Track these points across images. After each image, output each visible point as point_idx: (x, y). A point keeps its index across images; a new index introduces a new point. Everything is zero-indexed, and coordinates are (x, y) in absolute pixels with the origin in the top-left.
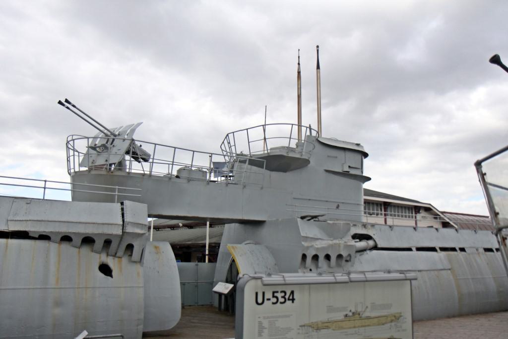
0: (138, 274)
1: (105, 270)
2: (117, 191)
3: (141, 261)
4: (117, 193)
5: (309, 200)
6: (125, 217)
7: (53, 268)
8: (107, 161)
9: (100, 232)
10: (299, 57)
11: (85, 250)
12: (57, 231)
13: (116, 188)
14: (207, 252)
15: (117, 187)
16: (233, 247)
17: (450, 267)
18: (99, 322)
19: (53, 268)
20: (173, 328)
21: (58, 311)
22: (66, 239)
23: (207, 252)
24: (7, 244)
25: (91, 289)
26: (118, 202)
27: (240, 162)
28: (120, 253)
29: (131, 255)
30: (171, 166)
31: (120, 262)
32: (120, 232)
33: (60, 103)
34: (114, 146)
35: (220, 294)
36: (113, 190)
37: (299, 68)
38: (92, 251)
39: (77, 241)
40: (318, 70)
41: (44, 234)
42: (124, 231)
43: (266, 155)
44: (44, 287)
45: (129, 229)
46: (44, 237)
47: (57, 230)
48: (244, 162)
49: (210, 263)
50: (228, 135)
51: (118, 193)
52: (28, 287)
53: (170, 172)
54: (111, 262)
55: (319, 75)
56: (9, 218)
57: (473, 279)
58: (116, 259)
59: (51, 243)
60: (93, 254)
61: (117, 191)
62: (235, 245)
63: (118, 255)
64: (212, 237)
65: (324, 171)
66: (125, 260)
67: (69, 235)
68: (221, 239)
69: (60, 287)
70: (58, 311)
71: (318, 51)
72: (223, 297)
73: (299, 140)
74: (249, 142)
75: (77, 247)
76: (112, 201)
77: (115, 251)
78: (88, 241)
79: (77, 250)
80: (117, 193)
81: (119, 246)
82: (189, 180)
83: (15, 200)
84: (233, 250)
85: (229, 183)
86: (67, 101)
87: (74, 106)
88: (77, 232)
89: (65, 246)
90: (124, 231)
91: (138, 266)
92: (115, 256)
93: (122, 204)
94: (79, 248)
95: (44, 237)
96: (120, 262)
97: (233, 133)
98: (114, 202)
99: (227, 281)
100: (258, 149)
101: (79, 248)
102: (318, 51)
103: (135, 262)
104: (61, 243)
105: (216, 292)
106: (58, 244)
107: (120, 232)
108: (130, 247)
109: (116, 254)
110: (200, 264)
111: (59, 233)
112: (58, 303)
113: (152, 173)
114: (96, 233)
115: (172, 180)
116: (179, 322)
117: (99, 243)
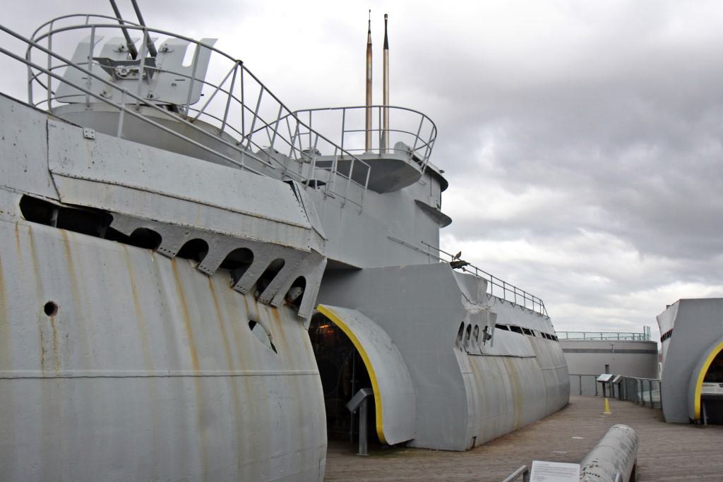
5: (402, 243)
10: (369, 21)
12: (185, 224)
17: (534, 355)
19: (179, 325)
30: (382, 109)
31: (277, 316)
35: (604, 383)
37: (369, 39)
38: (232, 287)
40: (386, 50)
41: (151, 227)
43: (376, 158)
44: (173, 372)
46: (146, 239)
47: (183, 221)
53: (313, 145)
55: (370, 66)
57: (556, 369)
59: (155, 254)
65: (414, 202)
66: (284, 312)
71: (386, 21)
73: (366, 150)
74: (343, 131)
88: (228, 233)
89: (187, 266)
92: (269, 304)
95: (146, 239)
97: (344, 108)
100: (355, 146)
102: (386, 21)
105: (600, 381)
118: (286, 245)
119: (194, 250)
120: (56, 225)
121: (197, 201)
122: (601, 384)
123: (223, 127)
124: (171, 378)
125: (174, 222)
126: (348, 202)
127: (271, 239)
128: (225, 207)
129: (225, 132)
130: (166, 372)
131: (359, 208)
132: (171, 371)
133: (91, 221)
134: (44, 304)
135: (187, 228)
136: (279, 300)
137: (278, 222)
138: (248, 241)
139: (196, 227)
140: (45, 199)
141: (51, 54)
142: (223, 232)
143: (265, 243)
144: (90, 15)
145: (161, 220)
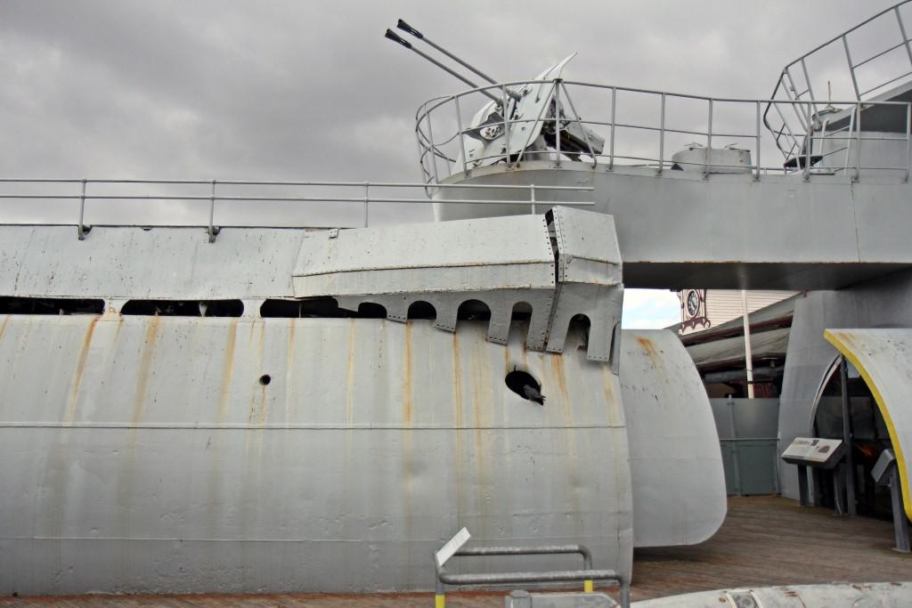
0: (608, 393)
1: (521, 382)
2: (533, 195)
3: (611, 361)
4: (533, 201)
6: (559, 245)
7: (395, 384)
8: (504, 150)
9: (500, 287)
11: (470, 338)
12: (398, 291)
13: (530, 189)
14: (750, 378)
15: (532, 186)
16: (843, 336)
18: (516, 515)
20: (701, 544)
21: (414, 485)
22: (421, 311)
23: (750, 378)
24: (293, 327)
25: (489, 432)
26: (537, 212)
27: (830, 128)
28: (557, 342)
29: (584, 348)
31: (558, 366)
32: (550, 283)
33: (390, 35)
34: (517, 117)
35: (802, 464)
36: (525, 194)
39: (448, 313)
42: (560, 280)
45: (572, 274)
46: (371, 310)
48: (843, 124)
49: (758, 400)
50: (787, 68)
51: (536, 199)
52: (341, 425)
54: (535, 365)
56: (295, 273)
58: (549, 357)
59: (387, 322)
60: (490, 347)
61: (533, 195)
62: (846, 331)
63: (550, 347)
64: (757, 347)
66: (570, 360)
67: (423, 299)
68: (786, 344)
69: (415, 426)
70: (414, 485)
72: (809, 470)
75: (449, 332)
76: (525, 210)
77: (543, 337)
78: (473, 313)
79: (451, 337)
80: (533, 201)
81: (552, 316)
82: (708, 174)
83: (307, 234)
84: (845, 343)
85: (811, 174)
86: (402, 25)
87: (419, 35)
89: (420, 329)
90: (560, 280)
91: (606, 373)
92: (543, 349)
93: (550, 217)
94: (455, 333)
95: (371, 310)
96: (558, 366)
98: (531, 213)
99: (817, 433)
101: (455, 333)
103: (596, 364)
104: (411, 323)
105: (789, 460)
106: (402, 326)
107: (550, 283)
108: (580, 325)
109: (546, 344)
110: (738, 401)
111: (402, 296)
112: (413, 467)
113: (615, 159)
114: (490, 288)
115: (665, 175)
116: (725, 521)
117: (501, 318)
118: (517, 287)
119: (421, 311)
120: (744, 282)
121: (410, 266)
122: (795, 467)
123: (612, 161)
124: (373, 431)
125: (386, 291)
126: (862, 172)
127: (500, 284)
128: (439, 265)
129: (715, 150)
130: (367, 425)
131: (903, 174)
132: (373, 424)
133: (323, 307)
134: (263, 375)
135: (401, 294)
136: (557, 342)
137: (506, 264)
138: (470, 292)
139: (410, 290)
140: (283, 298)
141: (770, 103)
142: (438, 289)
143: (490, 290)
144: (844, 34)
145: (374, 293)
